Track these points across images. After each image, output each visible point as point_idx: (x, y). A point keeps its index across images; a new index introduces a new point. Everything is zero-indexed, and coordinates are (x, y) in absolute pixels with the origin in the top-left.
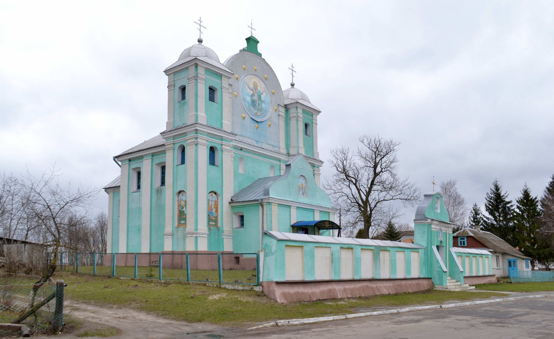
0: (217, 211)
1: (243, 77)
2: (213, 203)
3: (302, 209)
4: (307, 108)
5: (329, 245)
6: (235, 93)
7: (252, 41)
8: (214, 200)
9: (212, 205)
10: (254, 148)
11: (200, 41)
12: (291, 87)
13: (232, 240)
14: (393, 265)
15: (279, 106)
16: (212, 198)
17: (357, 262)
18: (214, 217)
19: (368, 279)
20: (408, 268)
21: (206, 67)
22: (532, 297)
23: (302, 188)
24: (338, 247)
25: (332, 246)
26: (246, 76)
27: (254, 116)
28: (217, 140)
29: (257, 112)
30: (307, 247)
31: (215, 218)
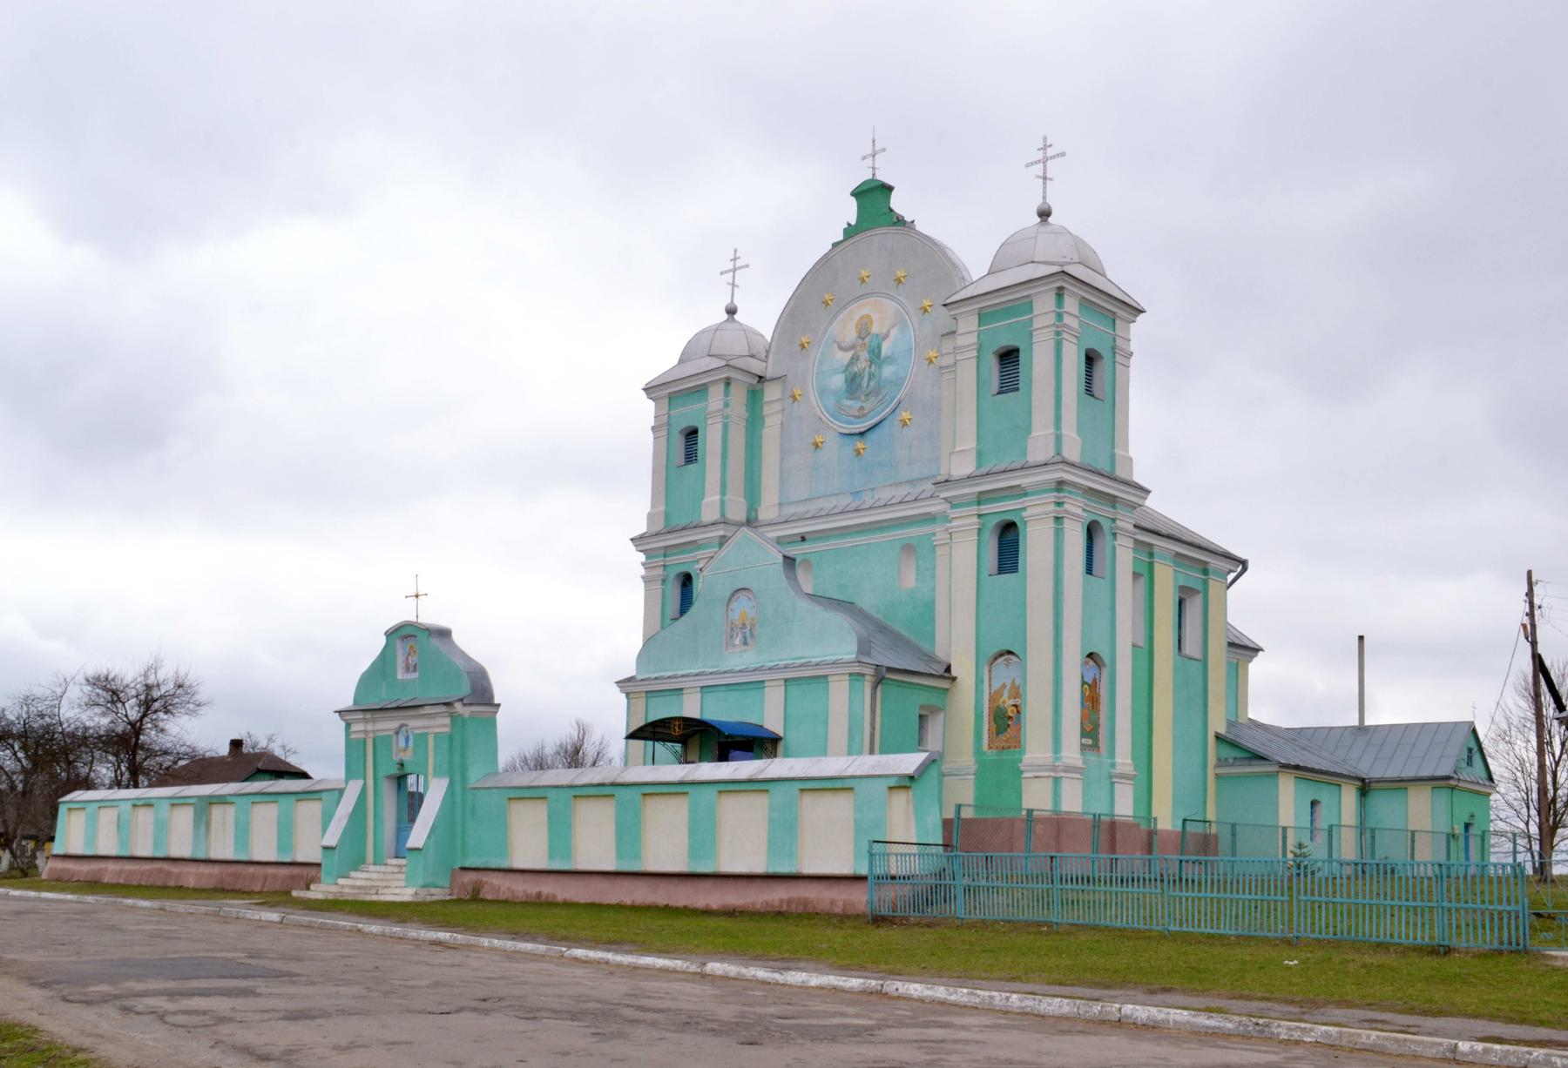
3: (724, 688)
5: (115, 804)
7: (873, 195)
10: (814, 524)
12: (1039, 220)
13: (1132, 787)
14: (243, 831)
17: (162, 829)
20: (92, 837)
22: (346, 926)
23: (744, 624)
24: (129, 805)
25: (121, 803)
27: (856, 420)
28: (686, 556)
29: (862, 404)
30: (91, 808)
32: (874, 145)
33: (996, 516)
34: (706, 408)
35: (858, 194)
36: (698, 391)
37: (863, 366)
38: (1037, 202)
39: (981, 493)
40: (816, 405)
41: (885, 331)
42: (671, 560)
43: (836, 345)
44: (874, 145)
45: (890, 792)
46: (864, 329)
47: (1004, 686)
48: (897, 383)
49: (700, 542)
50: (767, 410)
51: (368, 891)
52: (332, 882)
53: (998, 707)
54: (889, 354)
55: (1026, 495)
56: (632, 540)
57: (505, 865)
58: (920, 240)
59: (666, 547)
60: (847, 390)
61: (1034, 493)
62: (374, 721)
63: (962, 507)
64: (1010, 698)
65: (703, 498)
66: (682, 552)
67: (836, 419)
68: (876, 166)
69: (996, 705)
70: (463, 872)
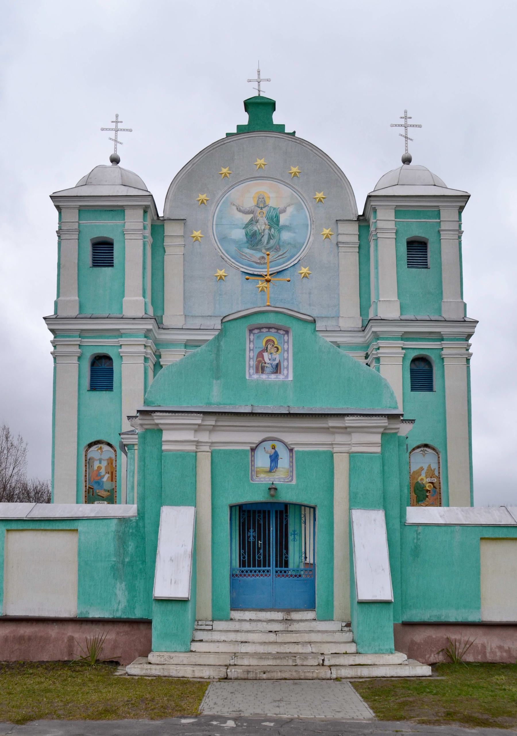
0: (113, 477)
1: (221, 193)
2: (104, 464)
4: (408, 201)
6: (195, 232)
8: (107, 457)
9: (99, 468)
11: (115, 160)
15: (339, 222)
16: (101, 454)
18: (105, 490)
19: (379, 601)
21: (80, 206)
26: (232, 187)
27: (257, 265)
31: (109, 493)
32: (259, 75)
33: (415, 351)
34: (124, 226)
35: (249, 105)
36: (112, 211)
37: (263, 228)
38: (401, 154)
39: (406, 333)
40: (217, 247)
41: (282, 206)
42: (87, 341)
43: (234, 208)
44: (259, 75)
45: (7, 533)
46: (261, 203)
47: (422, 469)
48: (297, 246)
49: (122, 331)
50: (167, 242)
51: (299, 662)
52: (183, 649)
53: (418, 482)
54: (287, 224)
55: (442, 340)
56: (45, 318)
57: (472, 618)
58: (311, 150)
59: (82, 330)
60: (247, 242)
61: (448, 340)
62: (213, 429)
63: (389, 340)
64: (427, 478)
65: (123, 297)
66: (100, 337)
67: (237, 261)
68: (261, 89)
69: (415, 481)
70: (407, 629)
